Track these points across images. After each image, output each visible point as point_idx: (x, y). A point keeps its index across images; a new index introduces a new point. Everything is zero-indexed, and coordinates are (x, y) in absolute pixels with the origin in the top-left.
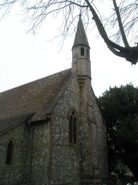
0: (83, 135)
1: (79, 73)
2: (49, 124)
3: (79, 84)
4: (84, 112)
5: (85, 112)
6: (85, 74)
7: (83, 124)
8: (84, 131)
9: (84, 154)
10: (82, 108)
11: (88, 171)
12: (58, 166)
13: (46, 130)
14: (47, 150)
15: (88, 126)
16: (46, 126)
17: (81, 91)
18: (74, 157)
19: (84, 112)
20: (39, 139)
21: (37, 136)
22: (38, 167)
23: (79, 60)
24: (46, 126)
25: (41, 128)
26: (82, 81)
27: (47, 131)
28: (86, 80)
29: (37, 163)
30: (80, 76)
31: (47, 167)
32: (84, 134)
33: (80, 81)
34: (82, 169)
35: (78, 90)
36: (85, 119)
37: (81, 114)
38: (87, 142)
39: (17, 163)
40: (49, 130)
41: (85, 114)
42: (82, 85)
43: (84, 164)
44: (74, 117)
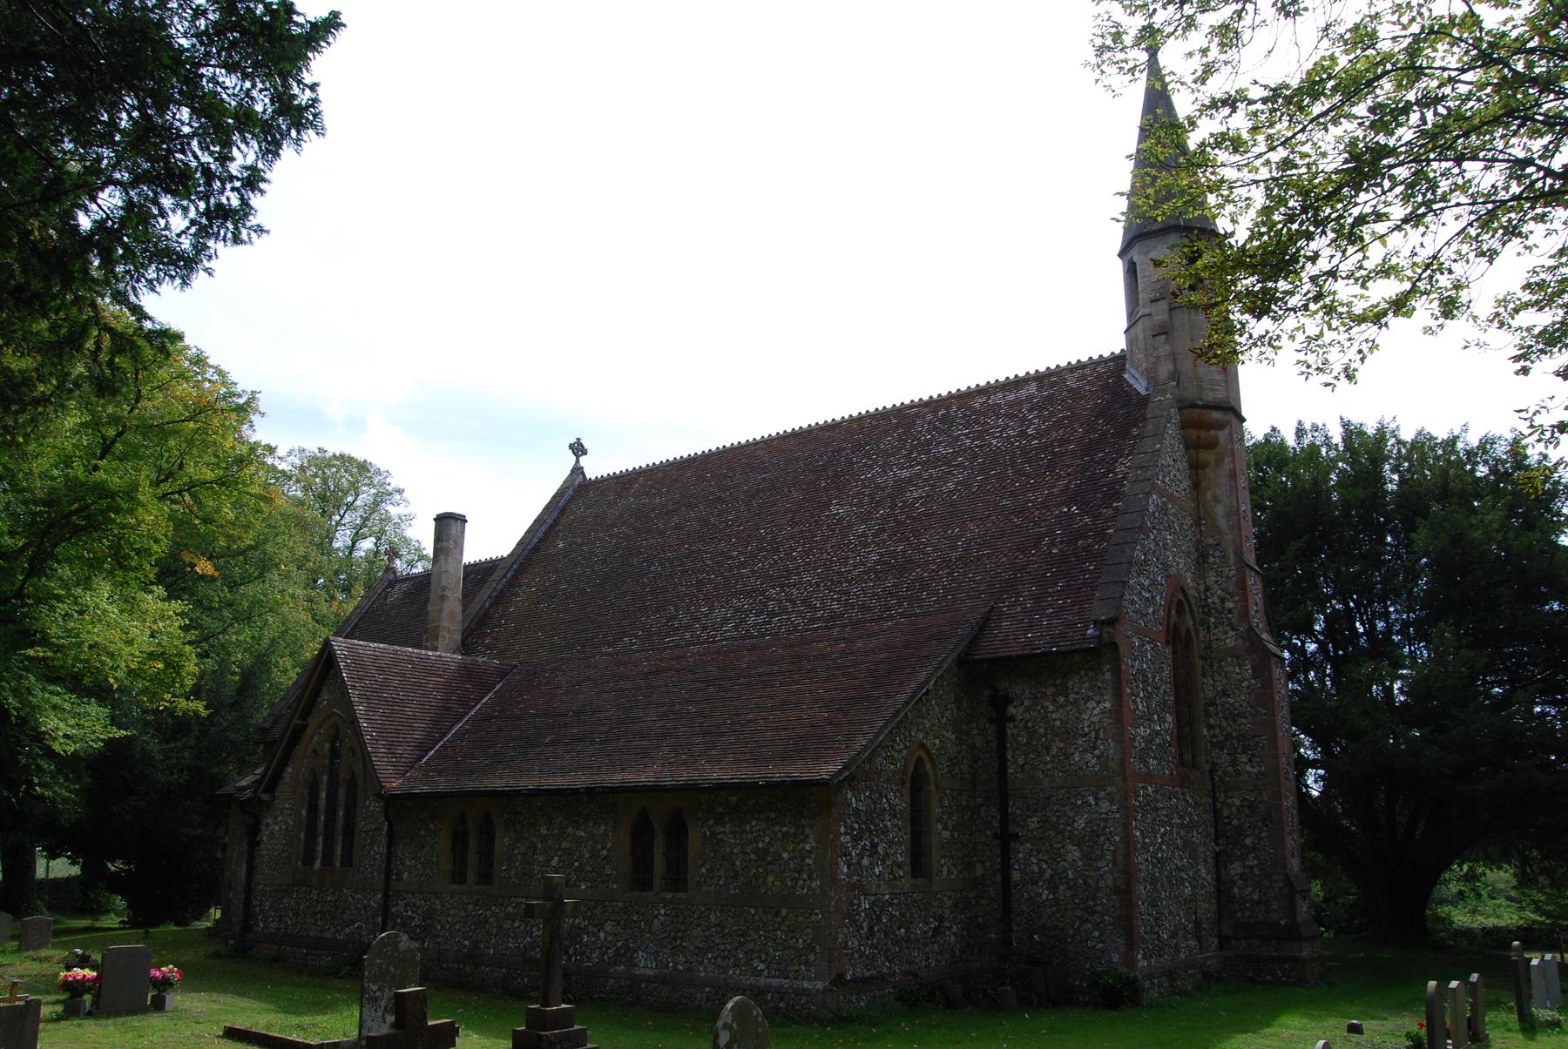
0: (1224, 724)
1: (1191, 393)
2: (1108, 676)
3: (1187, 448)
4: (1223, 600)
5: (1229, 605)
6: (1220, 394)
7: (1220, 667)
8: (1231, 700)
9: (1236, 822)
10: (1211, 578)
11: (1259, 903)
12: (1153, 881)
13: (1091, 704)
14: (1105, 806)
15: (1254, 677)
16: (1087, 685)
17: (1196, 485)
18: (1196, 837)
19: (1223, 600)
20: (1048, 748)
21: (1032, 733)
22: (1053, 889)
23: (1181, 318)
24: (1087, 685)
25: (1055, 695)
26: (1203, 433)
27: (1097, 709)
28: (1226, 431)
29: (1042, 871)
30: (1194, 406)
31: (1117, 890)
32: (1234, 717)
33: (1193, 434)
34: (1222, 890)
35: (1186, 484)
36: (1230, 642)
37: (1209, 614)
38: (1250, 761)
39: (945, 873)
40: (1108, 705)
41: (1230, 611)
42: (1207, 456)
43: (1236, 868)
44: (1183, 629)
